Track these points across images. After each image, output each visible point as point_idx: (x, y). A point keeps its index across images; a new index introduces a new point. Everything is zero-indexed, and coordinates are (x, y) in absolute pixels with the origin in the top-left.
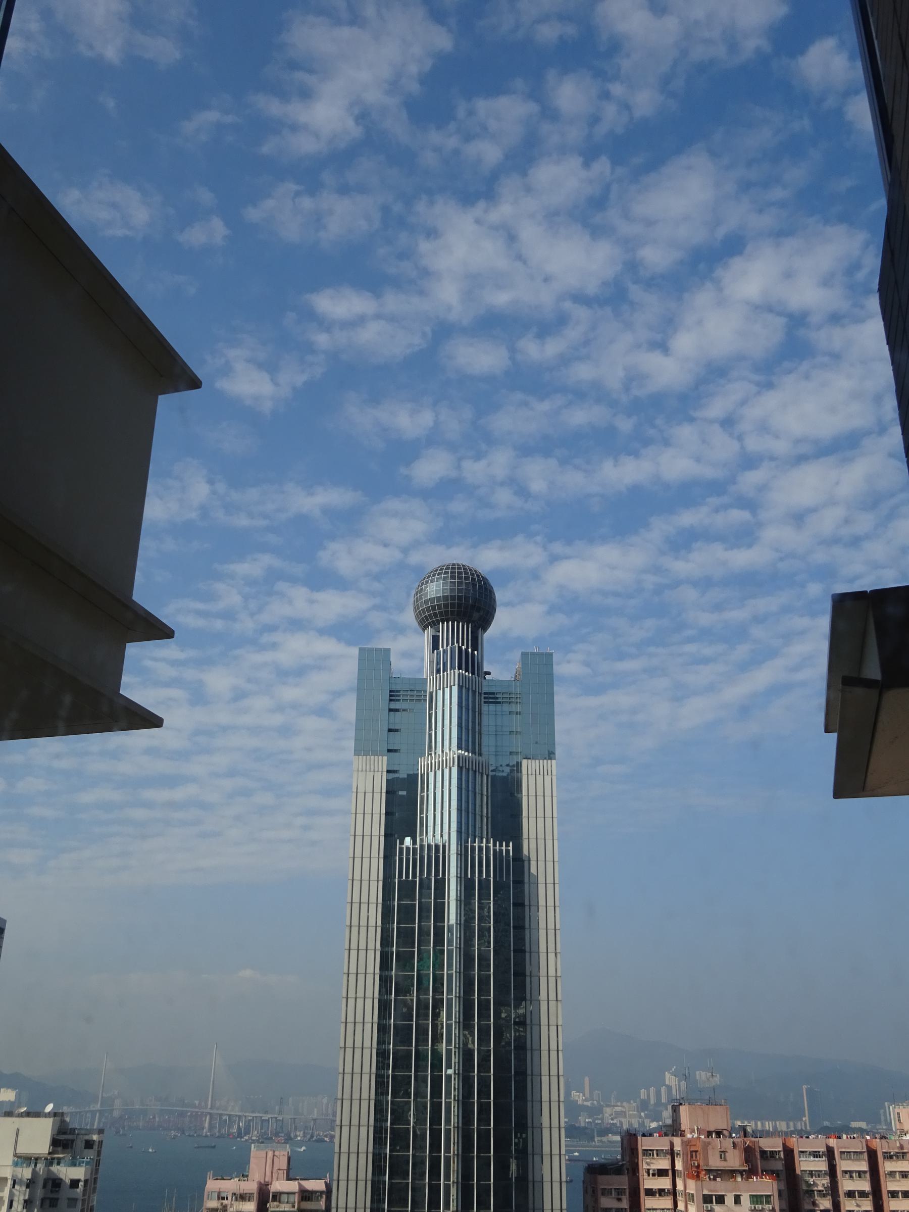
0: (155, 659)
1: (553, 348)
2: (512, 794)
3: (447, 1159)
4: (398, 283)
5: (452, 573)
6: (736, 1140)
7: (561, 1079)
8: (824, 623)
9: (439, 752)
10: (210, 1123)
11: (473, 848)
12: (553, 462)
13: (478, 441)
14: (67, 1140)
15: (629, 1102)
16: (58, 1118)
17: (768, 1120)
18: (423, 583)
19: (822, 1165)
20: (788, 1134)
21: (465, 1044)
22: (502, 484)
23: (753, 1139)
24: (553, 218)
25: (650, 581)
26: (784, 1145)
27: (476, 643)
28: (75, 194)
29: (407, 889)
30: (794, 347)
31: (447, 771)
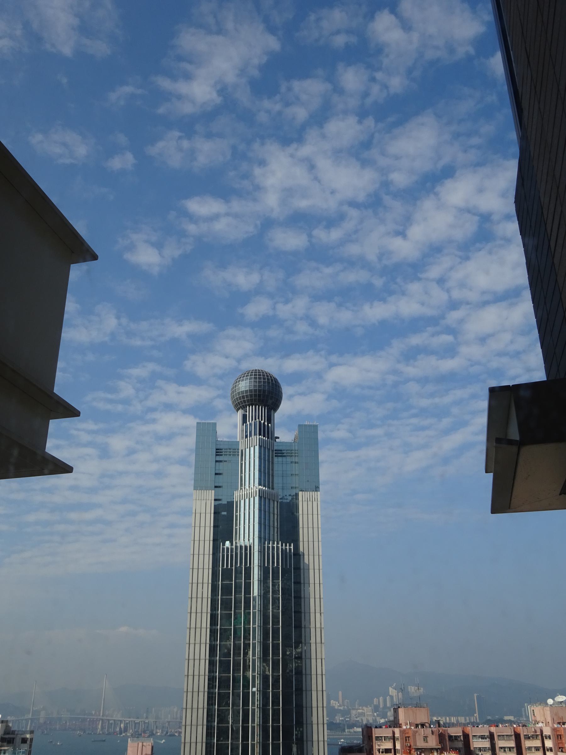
0: (78, 430)
1: (335, 235)
2: (293, 514)
3: (253, 745)
4: (240, 194)
5: (255, 375)
6: (433, 729)
7: (324, 693)
8: (484, 404)
9: (247, 487)
10: (102, 726)
11: (268, 548)
12: (333, 305)
13: (287, 292)
14: (10, 738)
15: (367, 707)
16: (4, 724)
17: (454, 716)
18: (237, 381)
19: (486, 744)
20: (465, 725)
21: (264, 671)
22: (301, 319)
23: (444, 728)
24: (338, 154)
25: (391, 379)
26: (463, 732)
27: (270, 419)
28: (39, 137)
29: (227, 574)
30: (483, 235)
31: (252, 499)
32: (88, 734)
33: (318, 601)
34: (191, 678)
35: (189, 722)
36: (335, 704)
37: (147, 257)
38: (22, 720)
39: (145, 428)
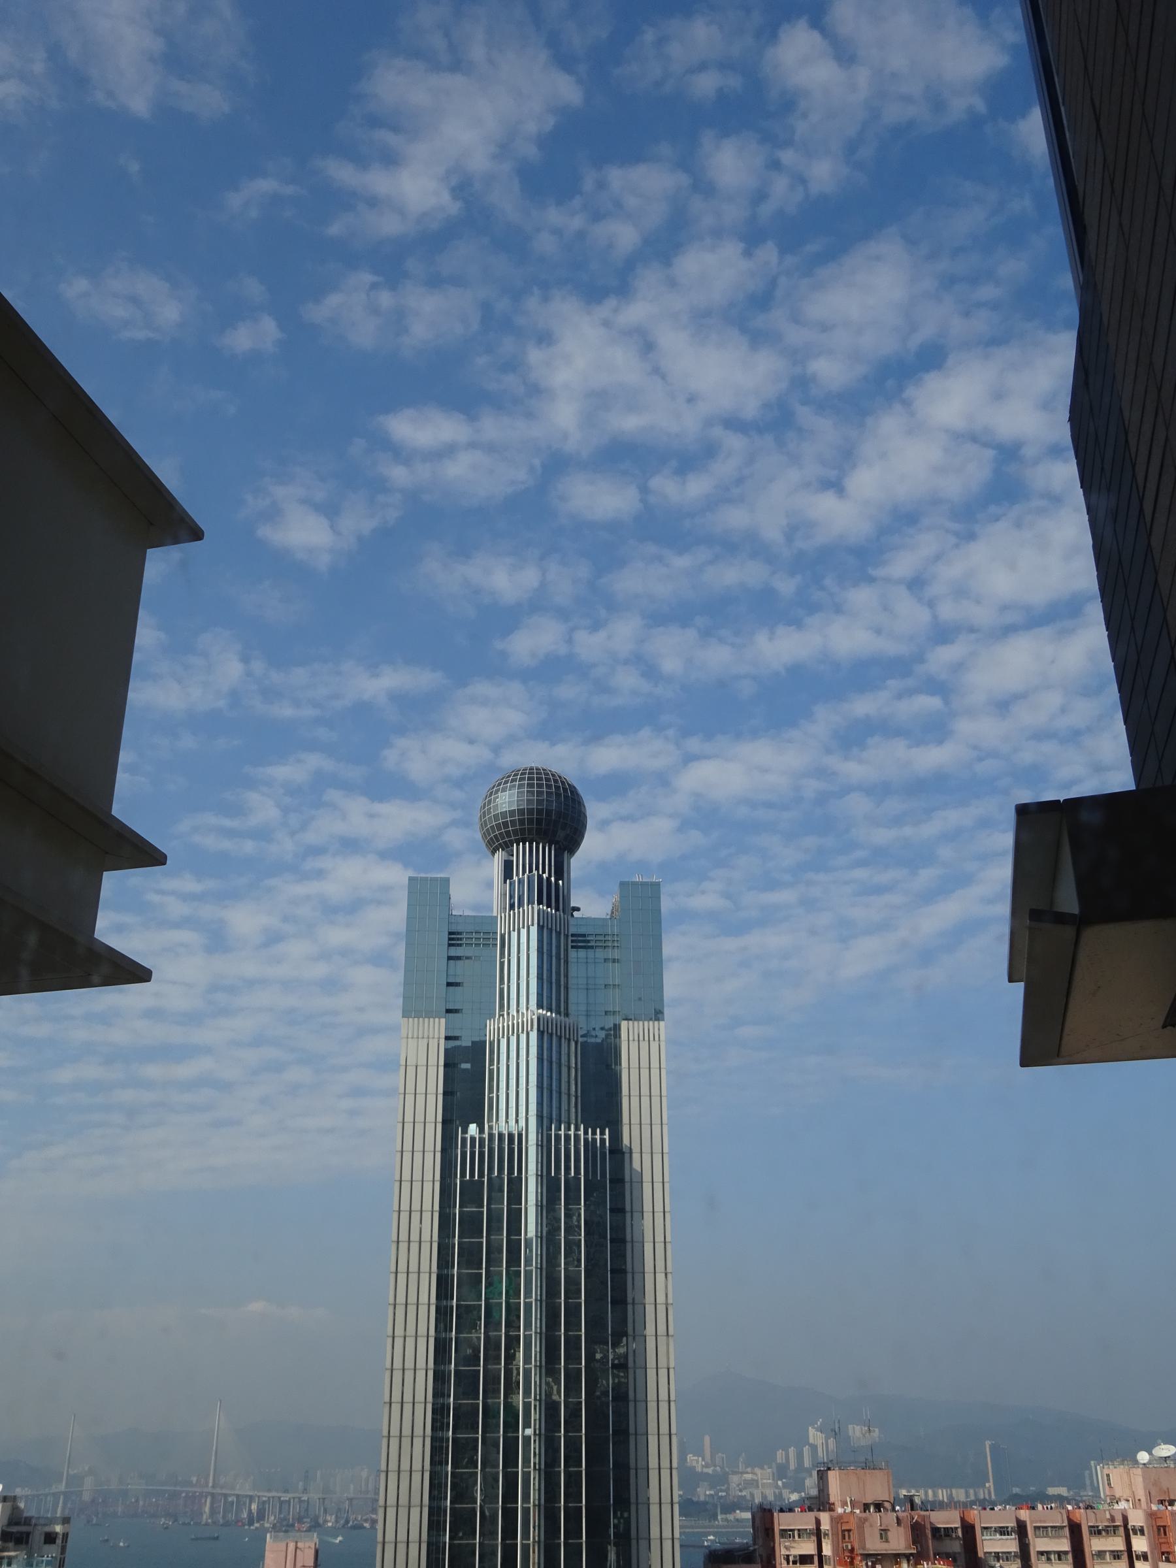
0: (162, 892)
1: (697, 487)
2: (608, 1066)
3: (526, 1548)
4: (499, 403)
5: (529, 779)
6: (901, 1514)
7: (674, 1439)
8: (1006, 840)
9: (513, 1012)
10: (212, 1507)
11: (558, 1137)
12: (691, 634)
13: (596, 606)
14: (22, 1533)
15: (762, 1468)
16: (9, 1504)
17: (942, 1487)
18: (492, 792)
19: (1011, 1545)
20: (967, 1506)
21: (549, 1395)
22: (626, 662)
23: (923, 1513)
24: (702, 321)
25: (812, 787)
26: (963, 1520)
27: (560, 871)
28: (82, 284)
29: (472, 1192)
30: (1004, 488)
31: (523, 1037)
32: (184, 1524)
33: (660, 1247)
34: (396, 1408)
35: (392, 1500)
36: (695, 1462)
37: (305, 533)
38: (46, 1495)
39: (301, 890)
